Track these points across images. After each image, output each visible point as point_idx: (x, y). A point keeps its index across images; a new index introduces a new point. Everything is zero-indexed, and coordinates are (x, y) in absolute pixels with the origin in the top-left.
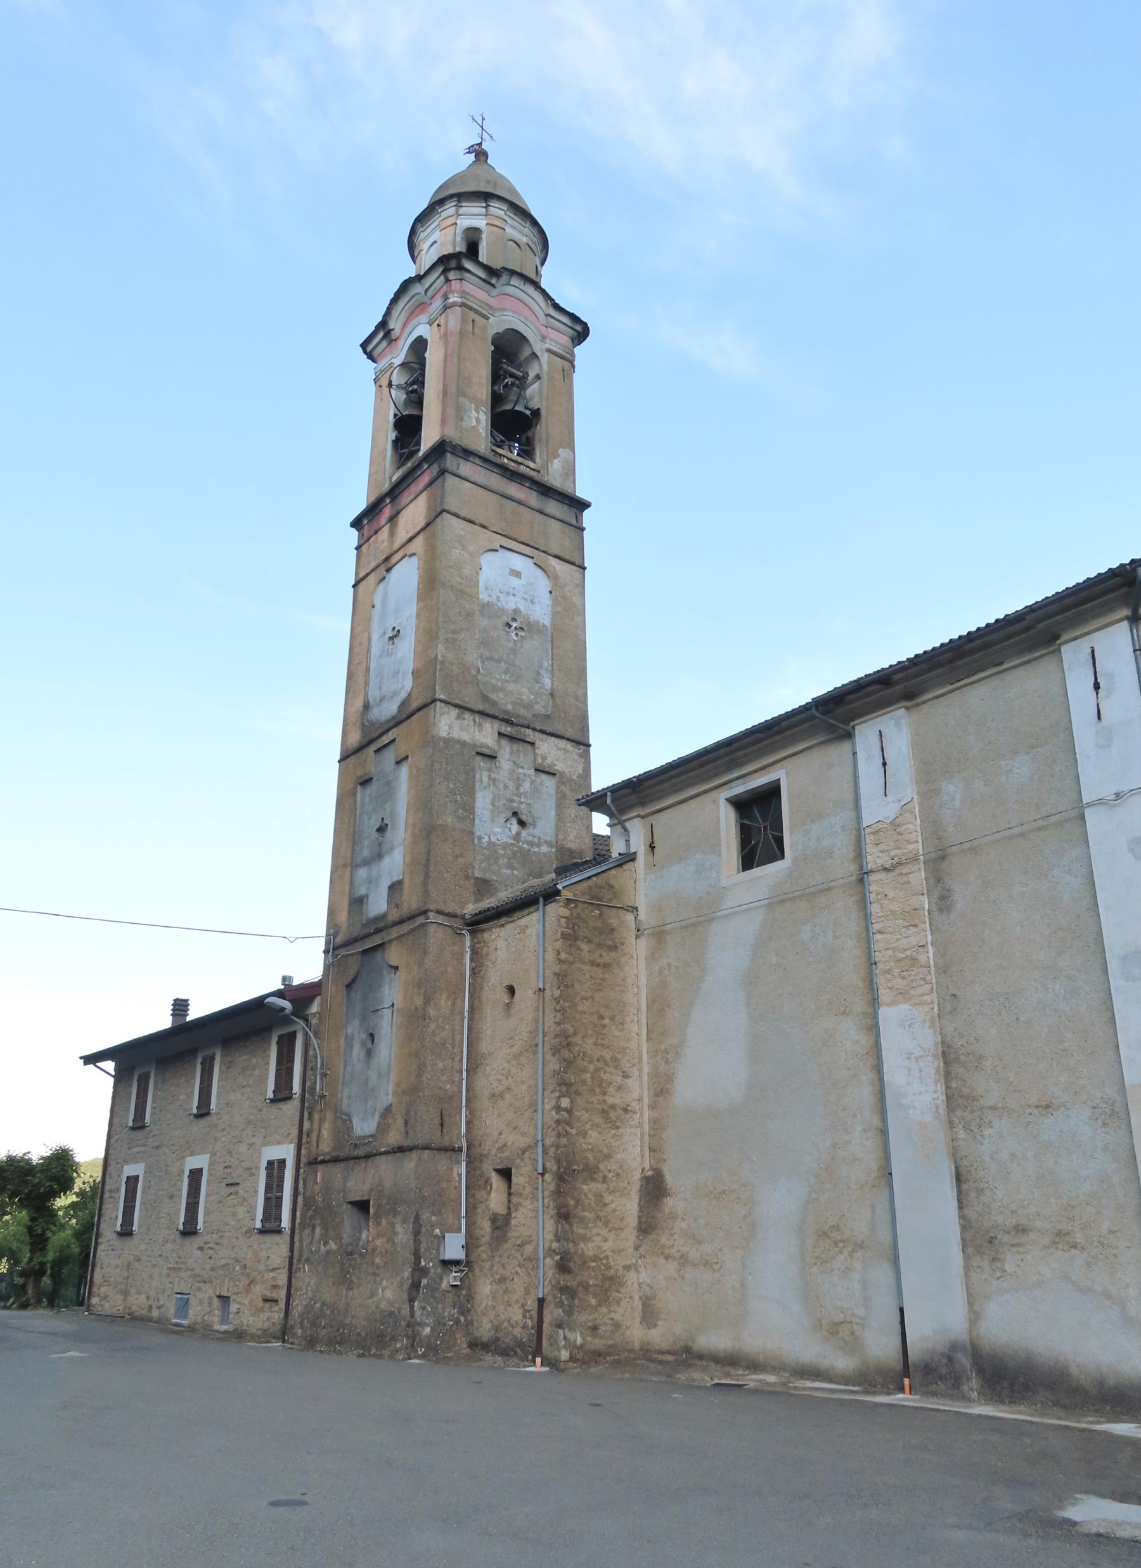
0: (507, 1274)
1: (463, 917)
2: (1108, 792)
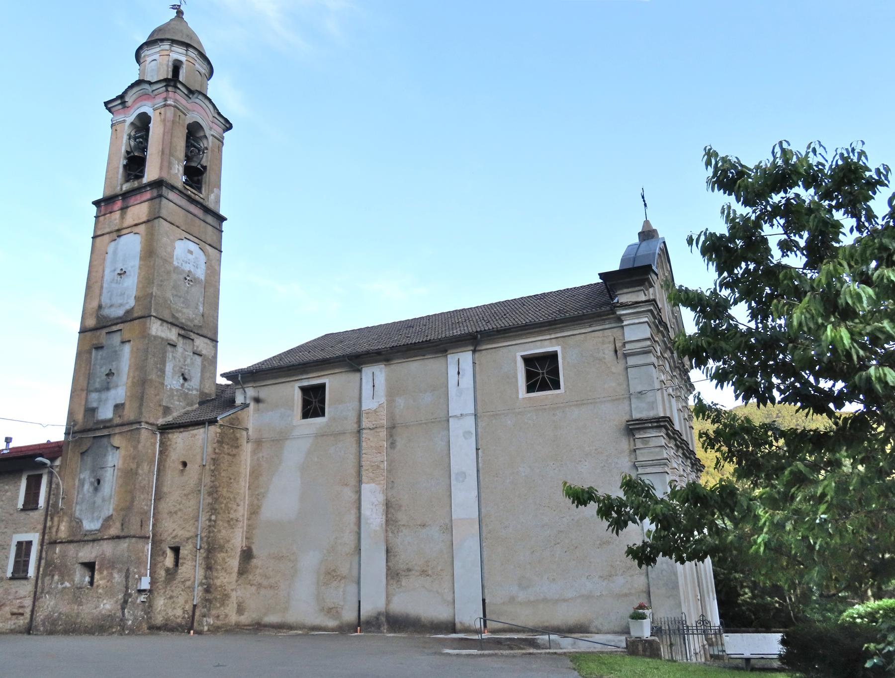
0: (174, 594)
1: (157, 425)
2: (458, 413)
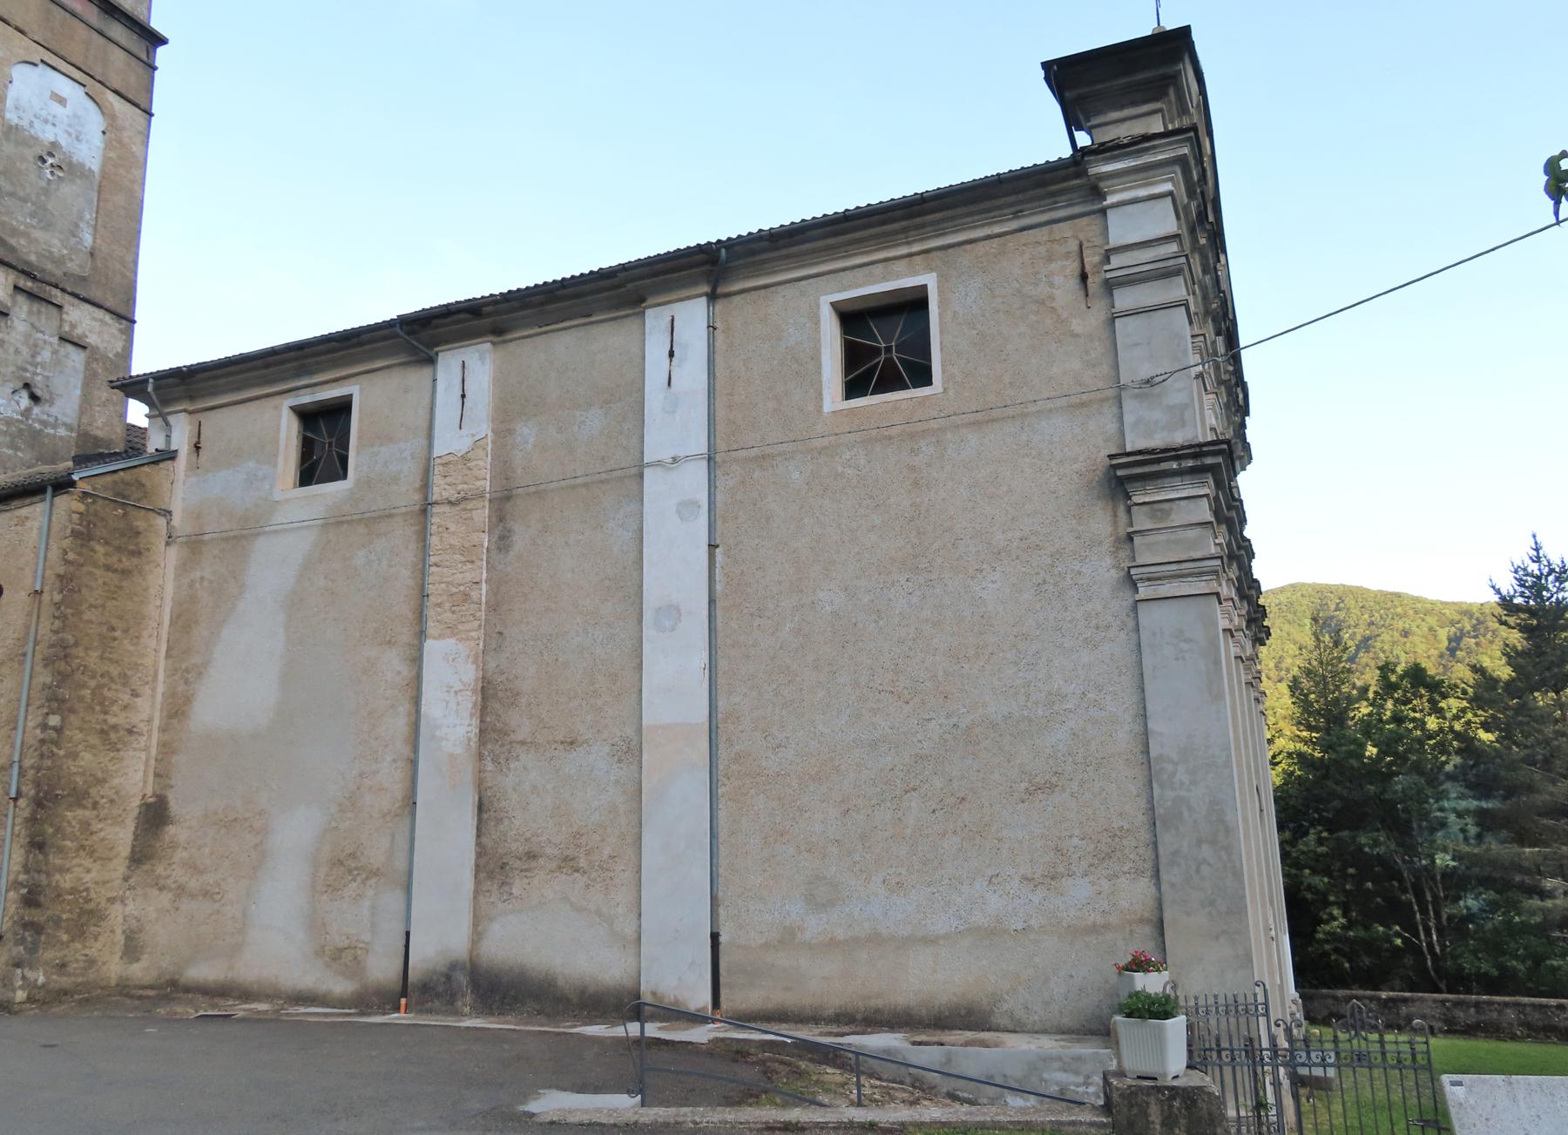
2: (666, 456)
